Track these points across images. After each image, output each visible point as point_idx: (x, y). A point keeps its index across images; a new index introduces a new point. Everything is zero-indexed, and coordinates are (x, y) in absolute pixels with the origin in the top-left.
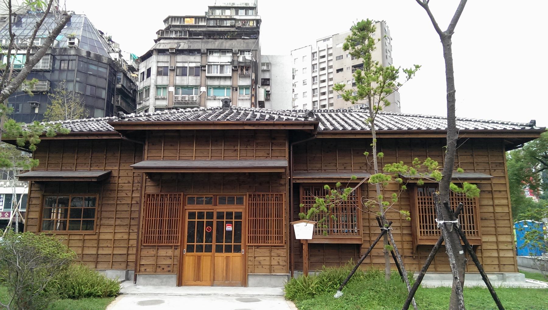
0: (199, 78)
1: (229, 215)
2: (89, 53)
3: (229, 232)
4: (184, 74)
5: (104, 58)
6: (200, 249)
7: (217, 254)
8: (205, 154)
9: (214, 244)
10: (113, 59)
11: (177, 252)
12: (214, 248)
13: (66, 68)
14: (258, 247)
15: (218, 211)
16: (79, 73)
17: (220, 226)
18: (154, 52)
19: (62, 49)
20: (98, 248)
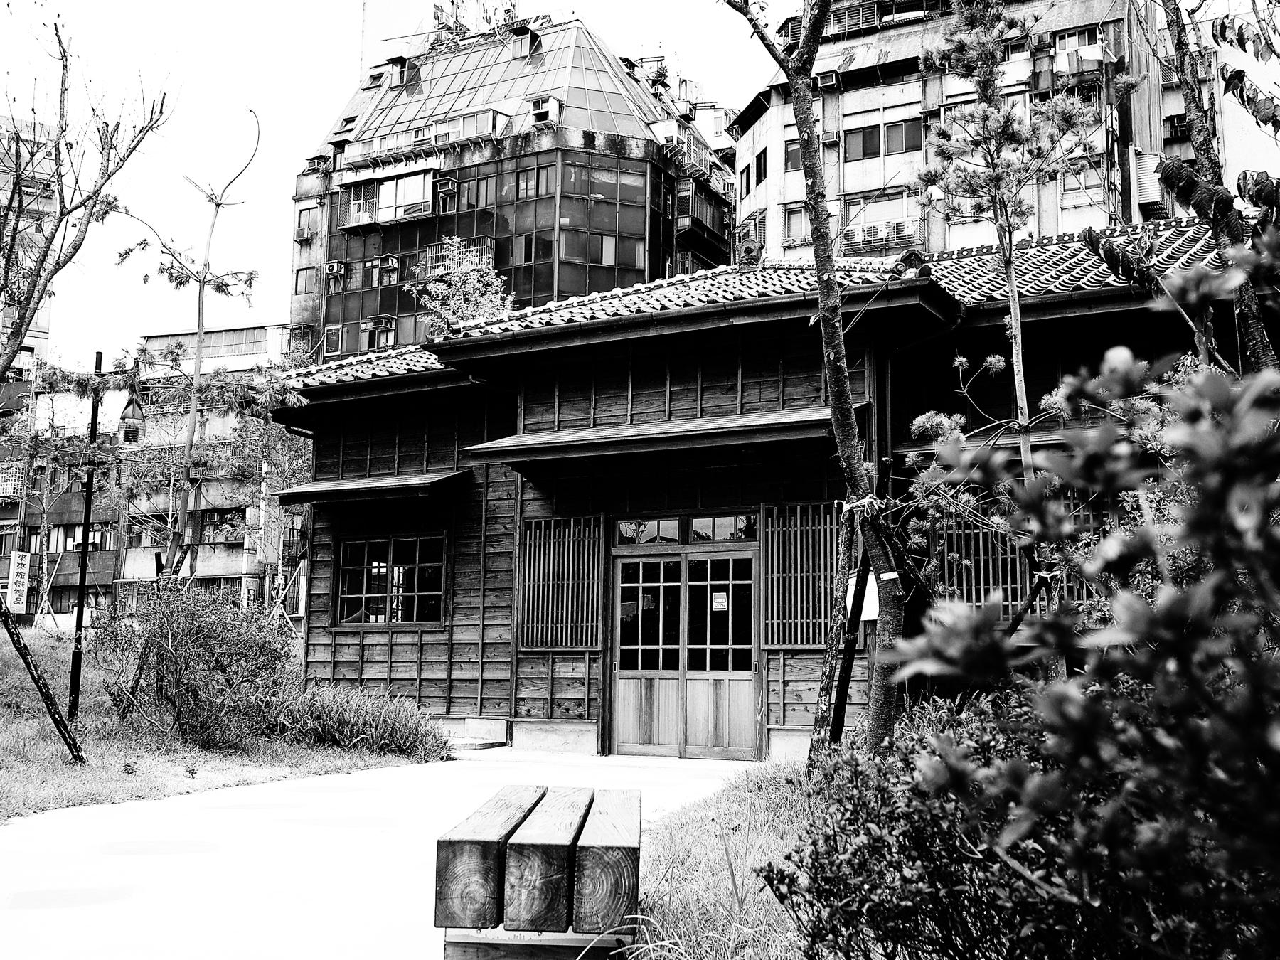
0: (919, 155)
1: (720, 568)
2: (589, 137)
3: (720, 616)
4: (870, 151)
5: (632, 143)
6: (650, 661)
7: (693, 674)
8: (657, 406)
9: (683, 647)
10: (663, 142)
11: (597, 668)
12: (683, 658)
13: (532, 193)
14: (793, 654)
15: (691, 558)
16: (566, 202)
17: (698, 597)
18: (774, 99)
19: (516, 138)
20: (451, 665)
